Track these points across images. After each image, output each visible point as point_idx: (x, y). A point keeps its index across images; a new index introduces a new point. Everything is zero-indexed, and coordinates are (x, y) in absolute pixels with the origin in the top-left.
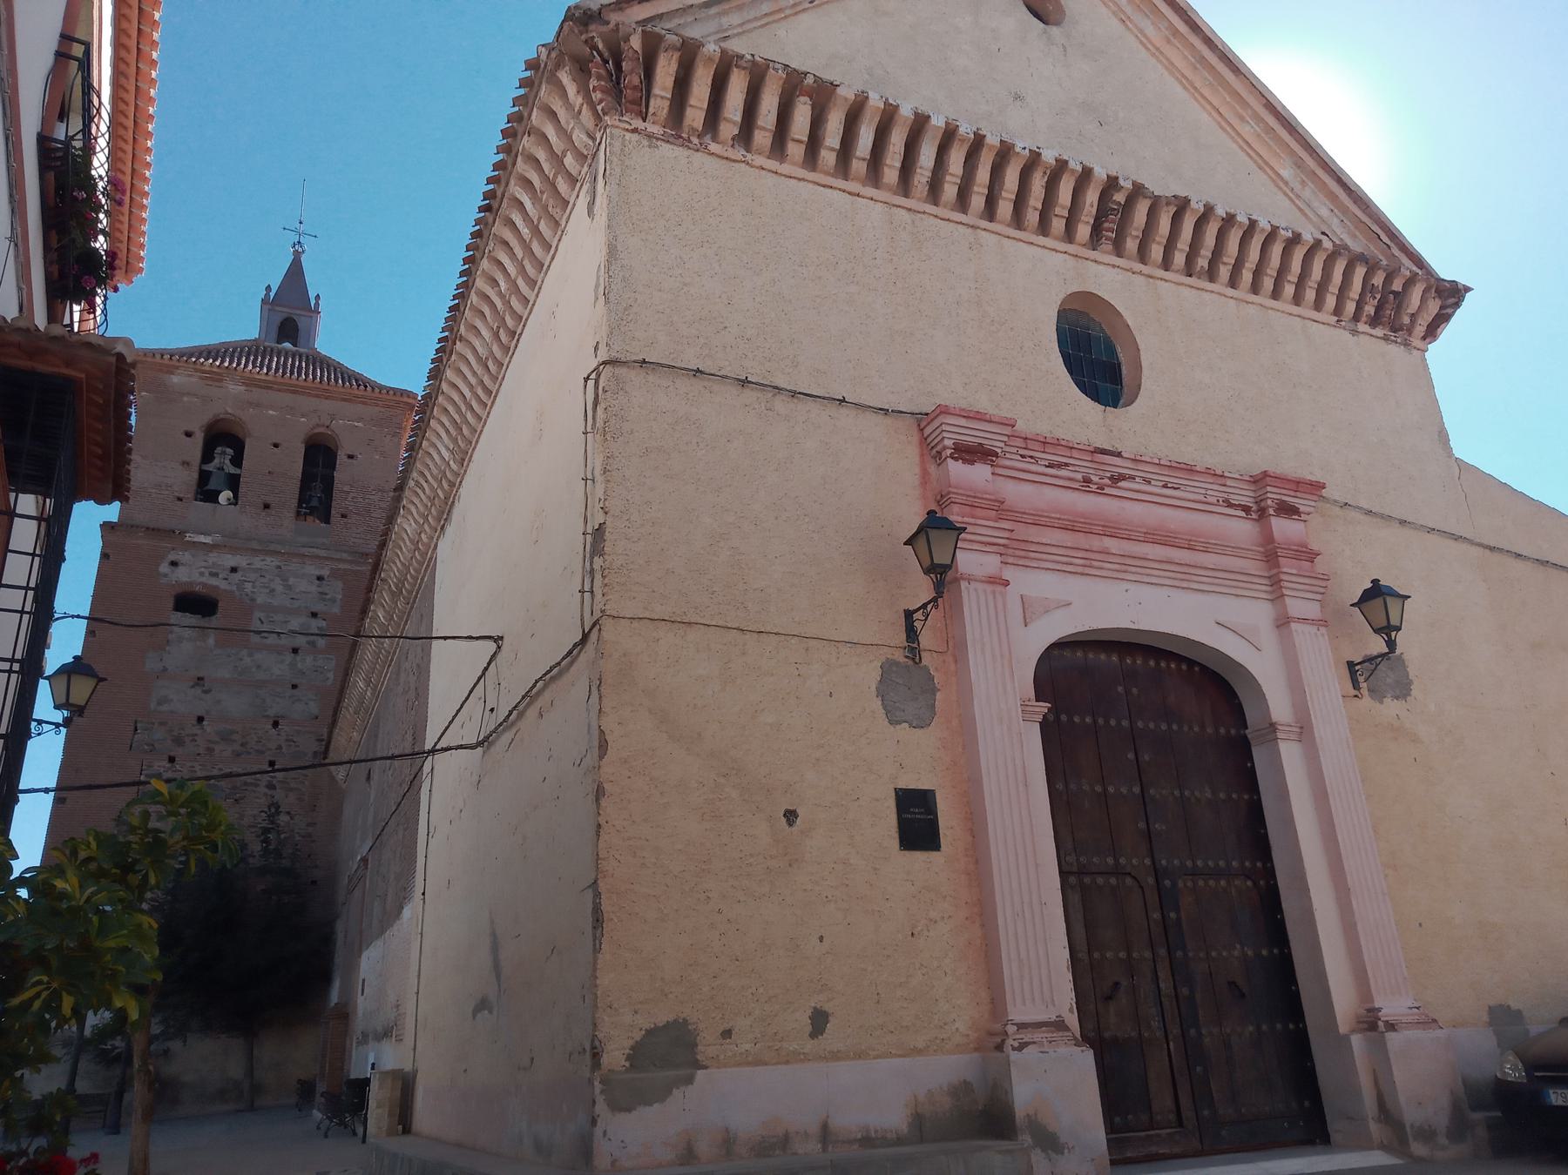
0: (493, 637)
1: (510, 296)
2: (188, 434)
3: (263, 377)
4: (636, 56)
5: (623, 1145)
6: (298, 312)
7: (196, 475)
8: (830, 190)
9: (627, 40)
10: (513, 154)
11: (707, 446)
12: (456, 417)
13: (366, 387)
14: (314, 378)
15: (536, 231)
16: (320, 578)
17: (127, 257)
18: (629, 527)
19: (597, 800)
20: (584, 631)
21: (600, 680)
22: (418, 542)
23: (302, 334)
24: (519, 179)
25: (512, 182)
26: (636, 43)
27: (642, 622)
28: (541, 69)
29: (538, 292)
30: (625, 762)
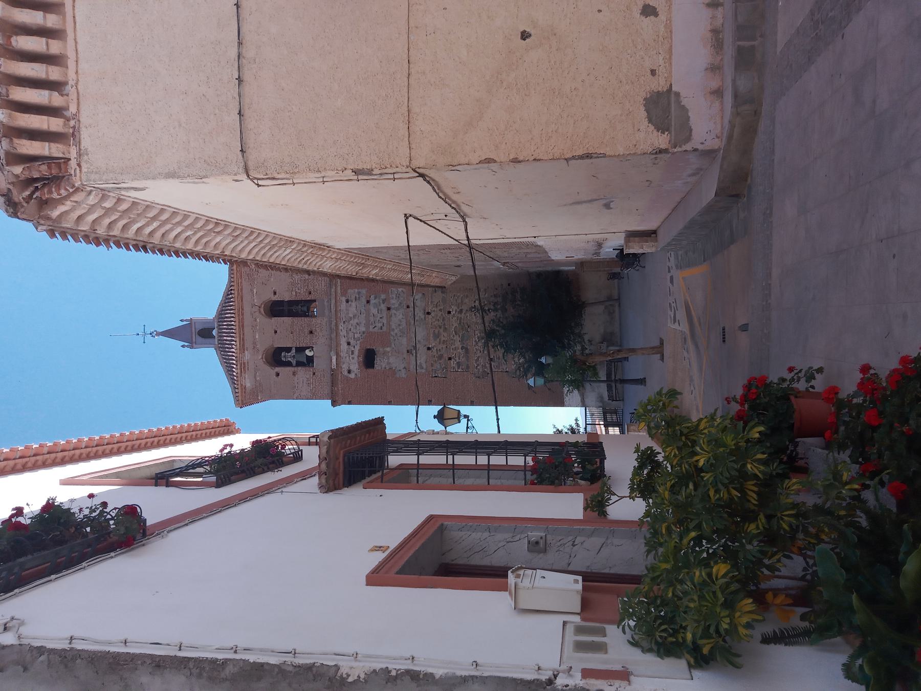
0: (405, 220)
1: (195, 228)
2: (278, 375)
3: (238, 343)
4: (26, 169)
5: (709, 132)
6: (193, 329)
7: (300, 368)
8: (77, 18)
9: (17, 176)
10: (109, 238)
11: (289, 105)
12: (267, 248)
13: (231, 290)
14: (233, 317)
15: (154, 219)
16: (347, 301)
17: (222, 427)
18: (353, 154)
19: (520, 162)
20: (418, 176)
21: (449, 165)
22: (336, 259)
23: (206, 326)
24: (123, 232)
25: (126, 236)
26: (18, 170)
27: (411, 142)
28: (53, 228)
29: (191, 212)
30: (497, 147)
